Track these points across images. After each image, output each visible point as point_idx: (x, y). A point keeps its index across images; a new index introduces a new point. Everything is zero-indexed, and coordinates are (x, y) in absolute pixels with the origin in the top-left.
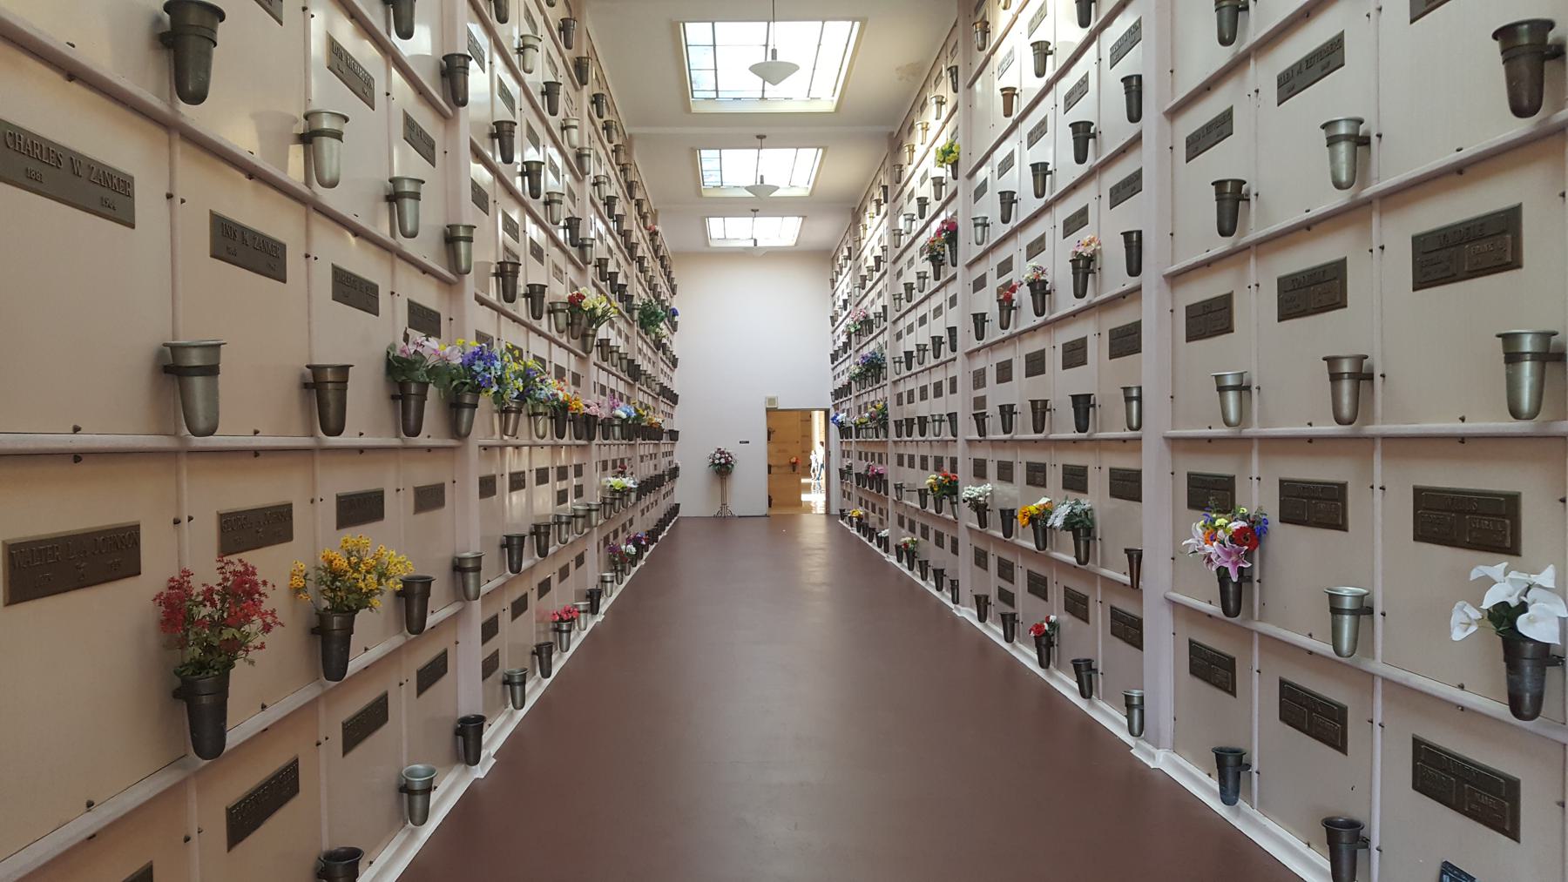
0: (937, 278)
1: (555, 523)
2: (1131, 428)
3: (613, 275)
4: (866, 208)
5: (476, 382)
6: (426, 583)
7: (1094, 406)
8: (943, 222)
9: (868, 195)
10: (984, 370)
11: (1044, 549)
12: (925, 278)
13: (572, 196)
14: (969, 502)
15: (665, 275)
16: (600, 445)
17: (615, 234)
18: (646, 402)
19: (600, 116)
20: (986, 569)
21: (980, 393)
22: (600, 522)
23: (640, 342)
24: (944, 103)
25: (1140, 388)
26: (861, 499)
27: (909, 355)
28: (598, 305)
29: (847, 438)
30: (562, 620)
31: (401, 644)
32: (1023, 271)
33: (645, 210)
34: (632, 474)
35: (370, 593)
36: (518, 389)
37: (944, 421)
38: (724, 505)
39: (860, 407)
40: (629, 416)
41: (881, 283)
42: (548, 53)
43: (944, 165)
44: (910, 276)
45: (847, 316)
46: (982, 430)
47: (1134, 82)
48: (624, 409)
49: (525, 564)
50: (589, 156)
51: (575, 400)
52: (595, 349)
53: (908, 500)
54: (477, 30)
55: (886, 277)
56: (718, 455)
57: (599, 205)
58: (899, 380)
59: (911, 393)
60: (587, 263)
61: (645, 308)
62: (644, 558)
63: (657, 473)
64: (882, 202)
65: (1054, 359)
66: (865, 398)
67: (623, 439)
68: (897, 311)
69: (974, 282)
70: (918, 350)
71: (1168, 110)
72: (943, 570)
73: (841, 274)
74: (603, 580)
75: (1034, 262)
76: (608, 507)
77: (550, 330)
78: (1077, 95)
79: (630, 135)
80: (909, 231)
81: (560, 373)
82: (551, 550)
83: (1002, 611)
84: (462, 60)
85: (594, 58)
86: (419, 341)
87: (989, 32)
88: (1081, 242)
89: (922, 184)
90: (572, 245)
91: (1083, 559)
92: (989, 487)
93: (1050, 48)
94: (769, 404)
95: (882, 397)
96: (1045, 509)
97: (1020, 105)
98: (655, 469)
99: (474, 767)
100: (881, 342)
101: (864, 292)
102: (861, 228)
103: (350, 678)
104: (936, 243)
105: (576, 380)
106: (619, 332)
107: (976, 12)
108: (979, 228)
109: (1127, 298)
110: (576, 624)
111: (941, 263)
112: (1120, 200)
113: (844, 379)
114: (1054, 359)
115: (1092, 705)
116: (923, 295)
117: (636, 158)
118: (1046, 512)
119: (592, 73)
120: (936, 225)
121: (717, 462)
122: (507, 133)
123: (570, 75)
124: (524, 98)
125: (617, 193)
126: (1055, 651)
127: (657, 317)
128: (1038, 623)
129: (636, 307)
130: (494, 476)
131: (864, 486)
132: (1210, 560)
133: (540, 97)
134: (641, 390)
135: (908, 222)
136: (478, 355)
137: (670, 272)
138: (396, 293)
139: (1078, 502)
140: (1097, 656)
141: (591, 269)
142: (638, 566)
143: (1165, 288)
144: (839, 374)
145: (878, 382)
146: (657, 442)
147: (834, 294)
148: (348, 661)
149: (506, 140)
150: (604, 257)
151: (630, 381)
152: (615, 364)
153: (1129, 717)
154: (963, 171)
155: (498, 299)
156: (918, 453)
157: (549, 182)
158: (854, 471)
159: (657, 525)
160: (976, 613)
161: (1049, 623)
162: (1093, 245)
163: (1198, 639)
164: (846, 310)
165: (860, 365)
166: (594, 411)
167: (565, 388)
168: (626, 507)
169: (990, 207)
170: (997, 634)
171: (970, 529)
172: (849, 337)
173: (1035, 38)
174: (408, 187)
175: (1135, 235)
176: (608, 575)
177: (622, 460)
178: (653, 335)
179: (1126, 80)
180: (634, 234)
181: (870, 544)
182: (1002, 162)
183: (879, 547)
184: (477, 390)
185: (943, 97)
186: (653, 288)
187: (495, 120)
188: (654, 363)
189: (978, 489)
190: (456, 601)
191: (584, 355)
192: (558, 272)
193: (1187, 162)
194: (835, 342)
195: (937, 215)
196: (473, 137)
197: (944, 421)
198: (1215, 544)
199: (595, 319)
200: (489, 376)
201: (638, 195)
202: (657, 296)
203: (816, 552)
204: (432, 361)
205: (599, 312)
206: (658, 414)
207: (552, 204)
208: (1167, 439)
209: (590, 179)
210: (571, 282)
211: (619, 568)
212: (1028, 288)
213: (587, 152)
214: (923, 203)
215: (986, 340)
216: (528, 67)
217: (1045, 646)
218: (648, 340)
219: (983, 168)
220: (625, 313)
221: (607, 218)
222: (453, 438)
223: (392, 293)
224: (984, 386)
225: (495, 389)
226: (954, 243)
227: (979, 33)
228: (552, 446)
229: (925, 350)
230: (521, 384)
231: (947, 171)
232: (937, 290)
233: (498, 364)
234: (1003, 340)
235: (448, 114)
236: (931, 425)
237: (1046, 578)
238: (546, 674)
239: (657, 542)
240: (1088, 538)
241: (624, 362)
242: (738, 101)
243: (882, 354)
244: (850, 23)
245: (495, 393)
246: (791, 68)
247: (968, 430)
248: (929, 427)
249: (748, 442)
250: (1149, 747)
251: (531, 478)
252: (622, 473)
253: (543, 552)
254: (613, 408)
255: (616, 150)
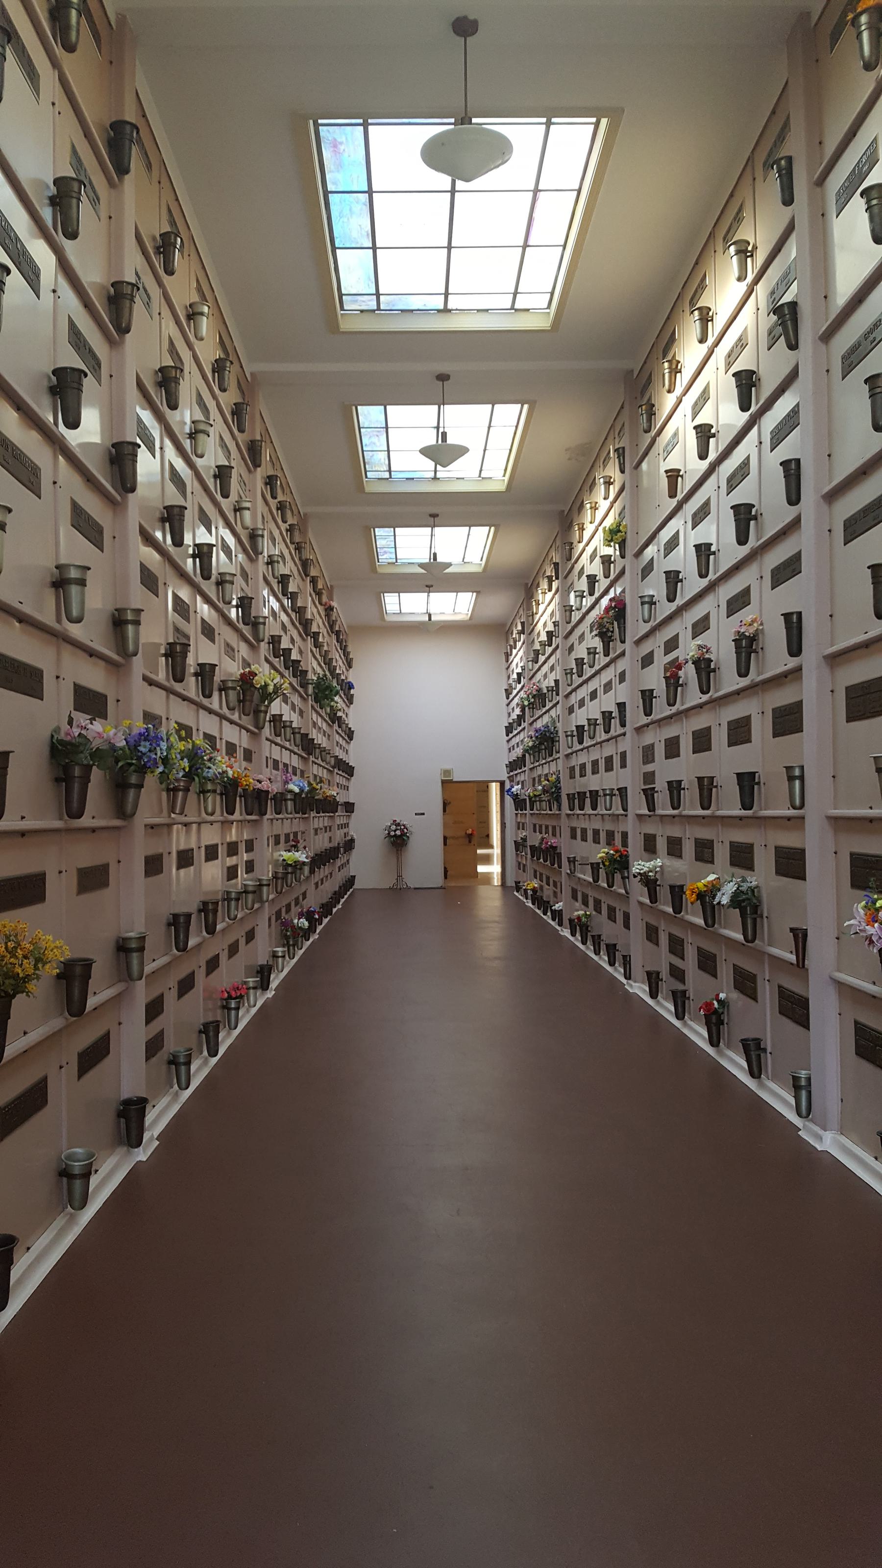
0: (606, 654)
1: (225, 900)
2: (794, 808)
3: (287, 651)
4: (539, 583)
5: (143, 763)
6: (87, 965)
7: (758, 783)
8: (611, 600)
9: (540, 572)
10: (653, 745)
11: (713, 926)
12: (595, 653)
13: (245, 575)
14: (639, 877)
15: (341, 649)
16: (272, 820)
17: (290, 611)
18: (321, 775)
19: (274, 497)
20: (657, 944)
21: (649, 768)
22: (271, 897)
23: (315, 716)
24: (612, 483)
25: (802, 768)
26: (535, 871)
27: (580, 728)
28: (270, 682)
29: (521, 810)
30: (230, 997)
31: (62, 1026)
32: (688, 649)
33: (320, 586)
34: (305, 848)
35: (27, 978)
36: (184, 769)
37: (615, 795)
38: (399, 876)
39: (534, 779)
40: (302, 790)
41: (553, 657)
42: (221, 437)
43: (612, 544)
44: (581, 652)
45: (522, 689)
46: (651, 806)
47: (793, 466)
48: (297, 783)
49: (192, 943)
50: (262, 536)
51: (246, 776)
52: (267, 724)
53: (581, 874)
54: (146, 416)
55: (558, 651)
56: (393, 827)
57: (272, 583)
58: (572, 754)
59: (583, 767)
60: (259, 640)
61: (320, 682)
62: (318, 931)
63: (332, 845)
64: (554, 578)
65: (720, 737)
66: (539, 771)
67: (296, 813)
68: (569, 685)
69: (642, 658)
70: (589, 725)
71: (827, 493)
72: (615, 945)
73: (515, 648)
74: (275, 956)
75: (699, 641)
76: (280, 881)
77: (221, 707)
78: (739, 477)
79: (305, 515)
80: (579, 607)
81: (231, 749)
82: (219, 927)
83: (674, 988)
84: (130, 447)
85: (268, 441)
86: (83, 724)
87: (655, 414)
88: (743, 623)
89: (591, 562)
90: (245, 623)
91: (750, 938)
92: (659, 862)
93: (713, 431)
94: (444, 777)
95: (555, 770)
96: (713, 885)
97: (685, 486)
98: (330, 841)
99: (136, 1150)
100: (554, 716)
101: (537, 666)
102: (534, 603)
103: (88, 1013)
104: (605, 620)
105: (248, 755)
106: (293, 707)
107: (643, 393)
108: (646, 606)
109: (790, 677)
110: (246, 1001)
111: (611, 639)
112: (780, 582)
113: (519, 751)
114: (720, 737)
115: (762, 1085)
116: (593, 671)
117: (310, 535)
118: (714, 889)
119: (266, 455)
120: (605, 602)
121: (392, 833)
122: (178, 517)
123: (243, 458)
124: (196, 483)
125: (291, 571)
126: (724, 1029)
127: (331, 691)
128: (708, 1001)
129: (310, 682)
130: (161, 855)
131: (538, 859)
132: (871, 942)
133: (212, 480)
134: (316, 763)
135: (578, 598)
136: (144, 736)
137: (346, 646)
138: (62, 677)
139: (744, 880)
140: (765, 1034)
141: (263, 646)
142: (311, 940)
143: (826, 671)
144: (513, 746)
145: (551, 755)
146: (332, 814)
147: (509, 667)
148: (4, 1047)
149: (177, 524)
150: (278, 634)
151: (304, 755)
152: (288, 738)
153: (797, 1098)
154: (630, 551)
155: (168, 679)
156: (591, 826)
157: (219, 561)
158: (529, 843)
159: (331, 898)
160: (647, 989)
161: (719, 1001)
162: (755, 625)
163: (863, 1020)
164: (519, 683)
165: (534, 739)
166: (265, 786)
167: (236, 765)
168: (298, 880)
169: (656, 587)
170: (669, 1011)
171: (641, 904)
172: (523, 710)
173: (699, 420)
174: (74, 574)
175: (795, 616)
176: (280, 950)
177: (295, 834)
178: (328, 709)
179: (785, 464)
180: (309, 611)
181: (545, 917)
182: (667, 542)
183: (554, 920)
184: (143, 770)
185: (611, 478)
186: (328, 662)
187: (166, 504)
188: (329, 736)
189: (647, 864)
190: (120, 981)
191: (256, 730)
192: (230, 650)
193: (845, 545)
194: (509, 714)
195: (606, 592)
196: (143, 523)
197: (615, 795)
198: (876, 925)
199: (266, 695)
200: (154, 756)
201: (313, 572)
202: (332, 670)
203: (490, 925)
204: (96, 744)
205: (271, 688)
206: (334, 785)
207: (224, 585)
208: (829, 818)
209: (263, 558)
210: (244, 660)
211: (291, 943)
212: (693, 666)
213: (260, 532)
214: (592, 580)
215: (654, 716)
216: (199, 452)
217: (716, 1024)
218: (324, 714)
219: (650, 547)
220: (299, 688)
221: (280, 596)
222: (118, 818)
223: (58, 677)
224: (653, 761)
225: (161, 769)
226: (622, 620)
227: (645, 415)
228: (222, 822)
229: (596, 724)
230: (187, 765)
231: (615, 549)
232: (607, 666)
233: (164, 745)
234: (671, 717)
235: (117, 500)
236: (603, 799)
237: (715, 955)
238: (213, 1053)
239: (331, 914)
240: (755, 916)
241: (298, 736)
242: (411, 481)
243: (555, 728)
244: (520, 405)
245: (161, 773)
246: (461, 451)
247: (637, 805)
248: (601, 800)
249: (423, 814)
250: (816, 1129)
251: (200, 855)
252: (295, 848)
253: (211, 930)
254: (286, 782)
255: (291, 529)
